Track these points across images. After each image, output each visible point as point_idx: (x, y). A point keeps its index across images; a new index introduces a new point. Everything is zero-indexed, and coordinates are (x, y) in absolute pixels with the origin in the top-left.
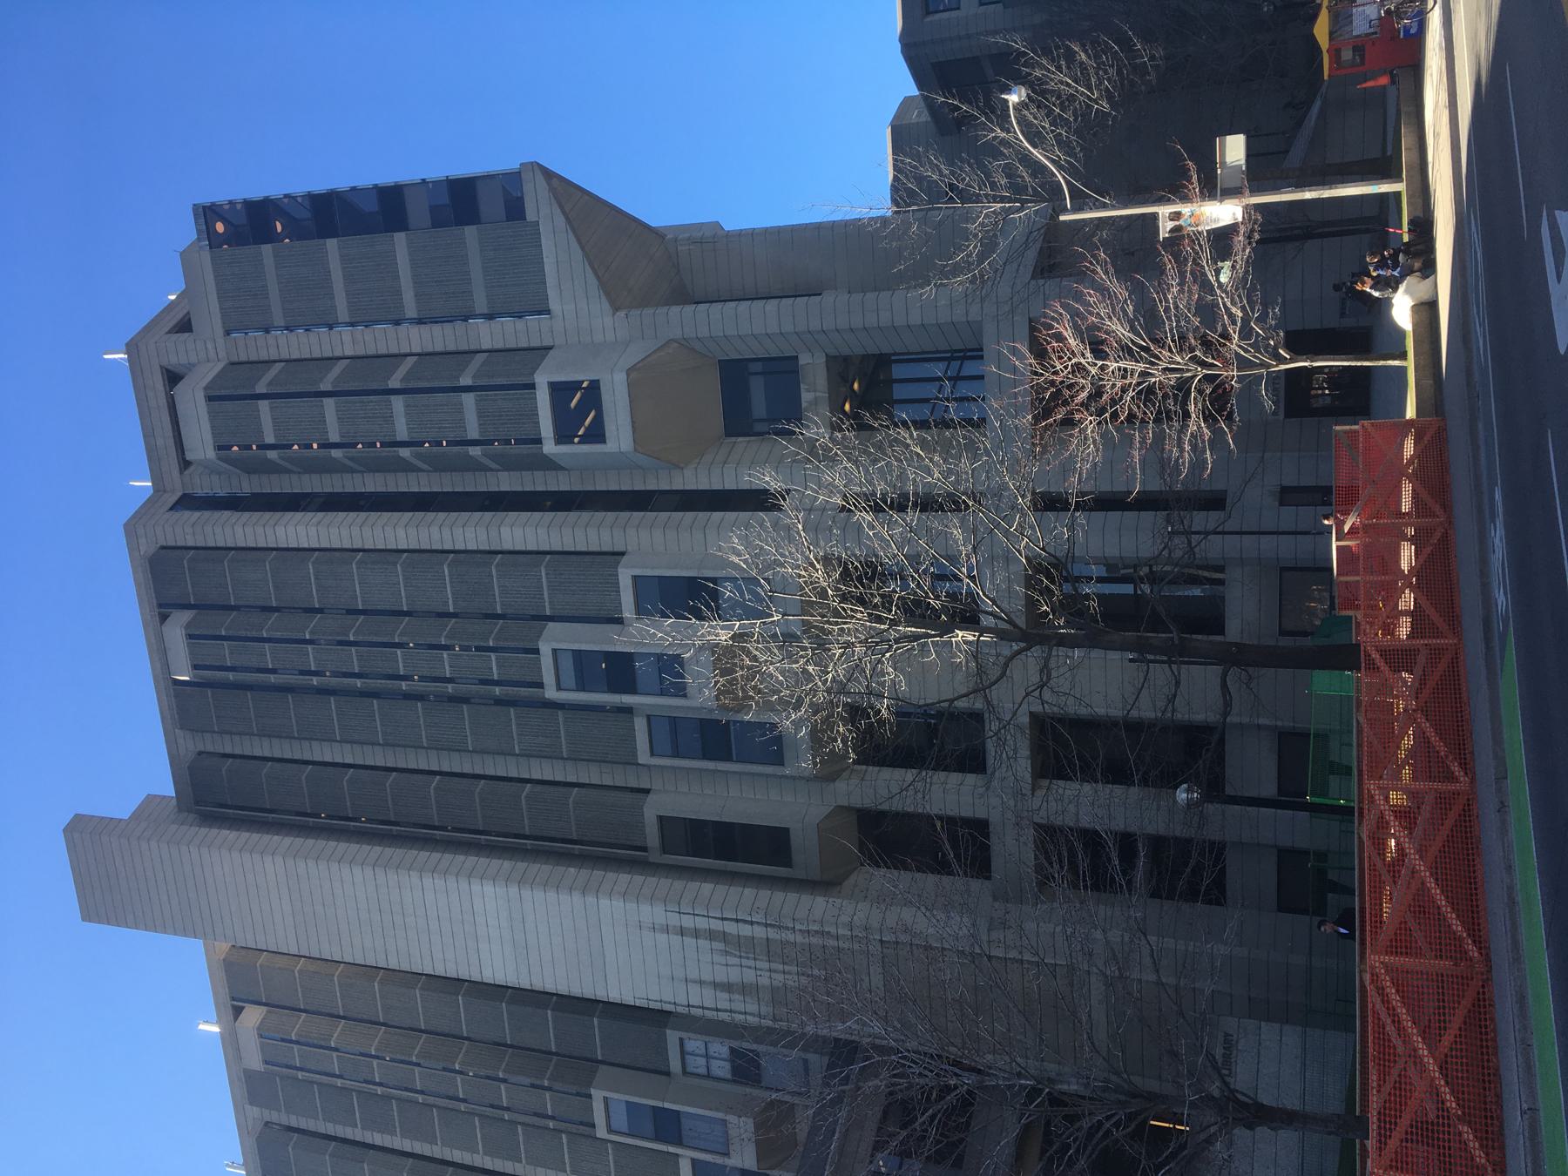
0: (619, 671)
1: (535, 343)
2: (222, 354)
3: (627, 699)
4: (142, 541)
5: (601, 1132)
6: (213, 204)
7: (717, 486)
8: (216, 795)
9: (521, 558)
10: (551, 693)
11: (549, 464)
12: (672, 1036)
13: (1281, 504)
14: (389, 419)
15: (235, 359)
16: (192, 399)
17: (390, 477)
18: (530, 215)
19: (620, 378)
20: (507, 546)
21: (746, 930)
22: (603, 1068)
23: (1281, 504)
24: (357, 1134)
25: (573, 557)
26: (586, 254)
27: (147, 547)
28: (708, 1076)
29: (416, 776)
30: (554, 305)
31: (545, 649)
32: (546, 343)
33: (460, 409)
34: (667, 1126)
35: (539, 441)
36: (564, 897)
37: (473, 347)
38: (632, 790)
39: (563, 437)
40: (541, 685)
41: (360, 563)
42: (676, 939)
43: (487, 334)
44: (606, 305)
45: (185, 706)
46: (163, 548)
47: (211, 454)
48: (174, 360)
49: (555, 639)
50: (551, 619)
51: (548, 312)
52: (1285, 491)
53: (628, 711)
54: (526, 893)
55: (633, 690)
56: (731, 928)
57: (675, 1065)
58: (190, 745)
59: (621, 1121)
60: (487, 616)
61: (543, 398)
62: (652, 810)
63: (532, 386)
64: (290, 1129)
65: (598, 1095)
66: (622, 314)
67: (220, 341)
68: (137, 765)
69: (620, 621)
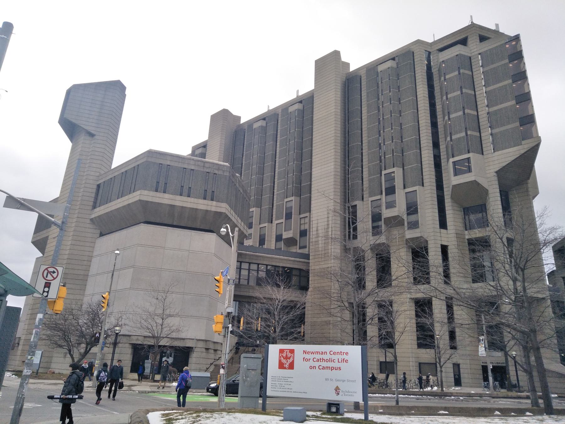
0: (391, 191)
1: (484, 149)
2: (473, 54)
3: (384, 193)
4: (415, 46)
5: (286, 200)
6: (520, 40)
7: (446, 208)
9: (419, 157)
10: (384, 172)
11: (448, 161)
12: (307, 214)
13: (453, 364)
14: (456, 111)
15: (472, 58)
16: (458, 50)
17: (441, 113)
18: (523, 142)
19: (473, 179)
20: (422, 153)
21: (330, 233)
22: (299, 198)
23: (453, 364)
24: (278, 138)
25: (421, 172)
26: (504, 167)
27: (414, 49)
28: (300, 224)
29: (360, 138)
30: (497, 153)
31: (394, 169)
32: (484, 153)
33: (460, 132)
34: (289, 216)
35: (453, 157)
36: (332, 187)
37: (481, 131)
38: (363, 196)
39: (454, 163)
40: (385, 169)
41: (414, 112)
42: (326, 216)
43: (486, 134)
44: (497, 169)
45: (372, 69)
46: (413, 52)
47: (441, 60)
48: (470, 41)
49: (398, 172)
50: (403, 169)
51: (494, 152)
52: (458, 365)
53: (382, 194)
54: (332, 177)
55: (386, 195)
56: (330, 229)
57: (302, 216)
58: (363, 73)
59: (289, 205)
60: (402, 150)
61: (466, 156)
62: (358, 203)
63: (469, 152)
64: (278, 121)
65: (293, 198)
66: (495, 174)
67: (477, 53)
68: (357, 59)
69: (405, 188)
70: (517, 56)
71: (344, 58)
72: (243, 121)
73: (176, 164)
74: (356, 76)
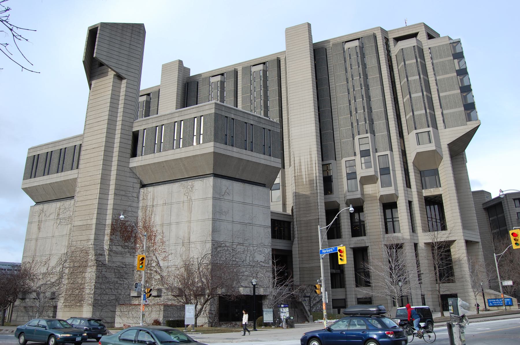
8: (319, 53)
14: (416, 92)
30: (447, 130)
35: (416, 129)
42: (308, 150)
70: (459, 56)
71: (185, 65)
72: (192, 74)
73: (239, 118)
74: (323, 48)
